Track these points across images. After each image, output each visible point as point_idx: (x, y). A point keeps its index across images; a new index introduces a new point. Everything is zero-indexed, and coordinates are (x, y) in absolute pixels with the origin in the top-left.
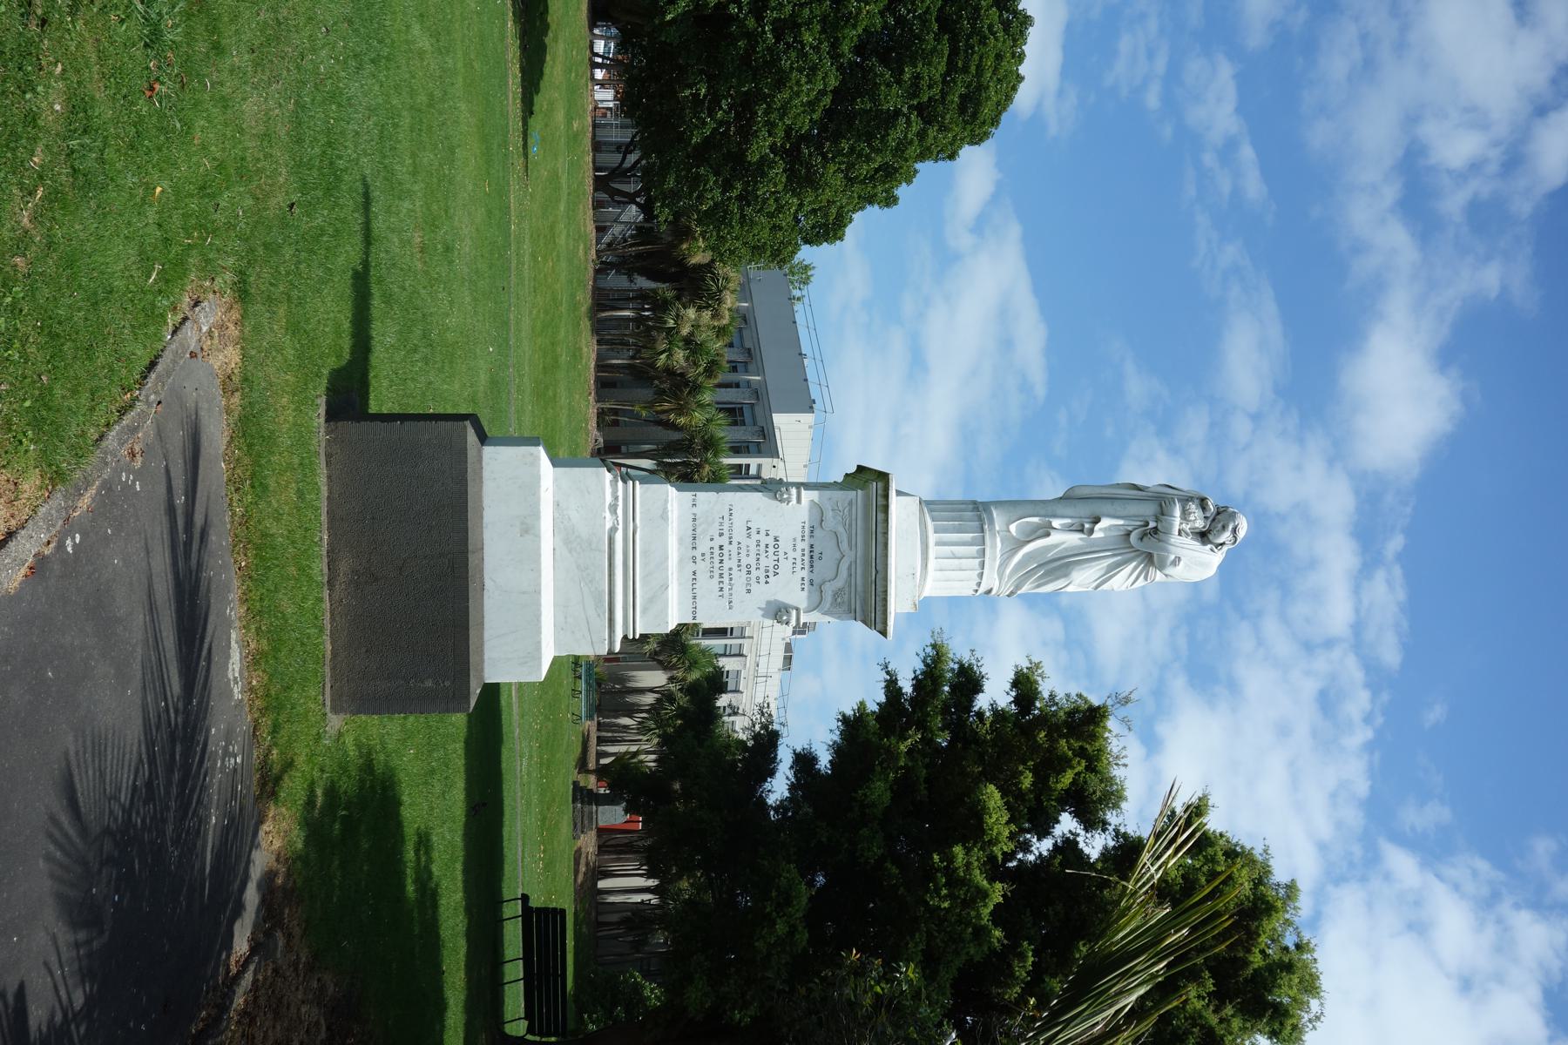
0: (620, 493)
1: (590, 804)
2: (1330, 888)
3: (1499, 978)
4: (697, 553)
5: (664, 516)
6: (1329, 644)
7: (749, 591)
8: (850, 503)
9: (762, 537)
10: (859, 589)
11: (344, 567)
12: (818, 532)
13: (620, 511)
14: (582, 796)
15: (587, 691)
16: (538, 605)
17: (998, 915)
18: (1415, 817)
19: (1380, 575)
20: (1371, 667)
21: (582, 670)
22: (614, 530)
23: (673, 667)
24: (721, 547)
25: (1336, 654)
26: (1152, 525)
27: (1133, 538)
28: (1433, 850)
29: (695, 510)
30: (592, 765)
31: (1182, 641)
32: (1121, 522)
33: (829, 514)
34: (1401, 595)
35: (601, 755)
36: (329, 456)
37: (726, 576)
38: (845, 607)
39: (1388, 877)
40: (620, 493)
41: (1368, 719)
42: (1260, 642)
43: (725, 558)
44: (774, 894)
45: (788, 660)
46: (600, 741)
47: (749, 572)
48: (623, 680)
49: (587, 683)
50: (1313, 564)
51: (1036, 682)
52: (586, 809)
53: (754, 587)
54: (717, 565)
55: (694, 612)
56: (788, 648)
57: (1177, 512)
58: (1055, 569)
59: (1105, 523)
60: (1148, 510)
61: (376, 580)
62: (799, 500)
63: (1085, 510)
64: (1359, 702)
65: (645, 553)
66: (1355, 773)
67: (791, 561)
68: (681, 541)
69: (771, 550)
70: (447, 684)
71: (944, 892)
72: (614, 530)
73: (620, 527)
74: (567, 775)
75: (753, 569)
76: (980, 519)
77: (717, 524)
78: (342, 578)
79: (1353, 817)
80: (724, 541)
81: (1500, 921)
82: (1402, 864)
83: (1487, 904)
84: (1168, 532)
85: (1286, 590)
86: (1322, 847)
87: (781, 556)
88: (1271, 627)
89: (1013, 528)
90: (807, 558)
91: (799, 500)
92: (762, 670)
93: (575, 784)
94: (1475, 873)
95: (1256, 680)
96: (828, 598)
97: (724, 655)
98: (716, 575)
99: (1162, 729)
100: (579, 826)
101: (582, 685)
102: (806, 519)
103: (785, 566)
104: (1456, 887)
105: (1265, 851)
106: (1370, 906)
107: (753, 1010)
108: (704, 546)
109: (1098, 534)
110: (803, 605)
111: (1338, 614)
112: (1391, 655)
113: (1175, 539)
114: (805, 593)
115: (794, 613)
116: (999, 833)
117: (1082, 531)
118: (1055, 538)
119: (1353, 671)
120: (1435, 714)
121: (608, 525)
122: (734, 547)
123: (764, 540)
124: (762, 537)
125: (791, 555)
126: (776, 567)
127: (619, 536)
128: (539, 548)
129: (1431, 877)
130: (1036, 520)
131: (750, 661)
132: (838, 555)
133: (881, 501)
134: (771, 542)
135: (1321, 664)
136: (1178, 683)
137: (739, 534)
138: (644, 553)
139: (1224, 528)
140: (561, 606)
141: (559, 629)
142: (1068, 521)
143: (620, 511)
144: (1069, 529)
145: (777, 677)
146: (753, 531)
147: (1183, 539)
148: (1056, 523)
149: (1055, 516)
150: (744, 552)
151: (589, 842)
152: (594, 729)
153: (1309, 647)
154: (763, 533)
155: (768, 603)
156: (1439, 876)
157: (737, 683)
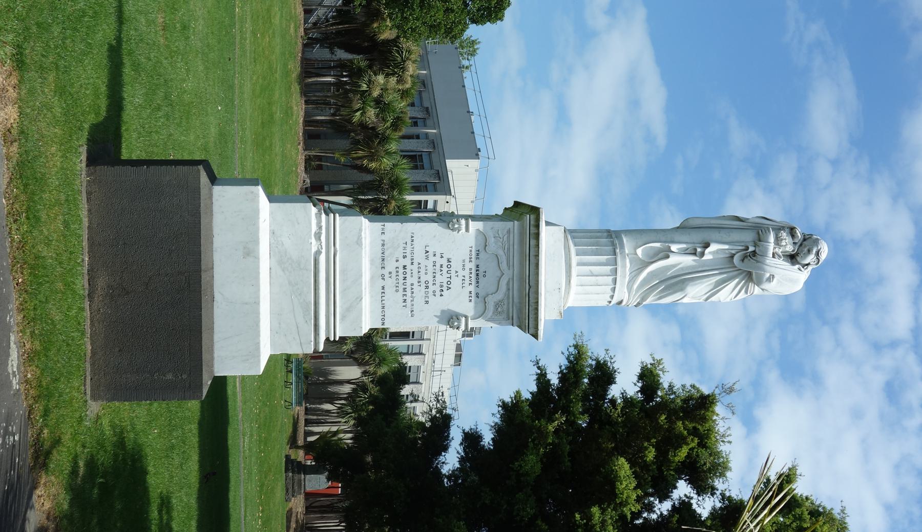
0: (323, 224)
1: (299, 473)
4: (386, 272)
5: (359, 242)
6: (894, 344)
7: (427, 302)
8: (509, 232)
10: (516, 300)
11: (101, 283)
12: (481, 255)
14: (292, 466)
15: (297, 382)
16: (257, 313)
22: (318, 253)
24: (404, 267)
25: (900, 352)
26: (751, 249)
27: (736, 260)
29: (383, 237)
30: (301, 442)
31: (775, 343)
32: (726, 247)
33: (491, 241)
36: (89, 194)
37: (409, 290)
38: (505, 316)
40: (323, 224)
43: (408, 276)
45: (458, 358)
47: (427, 287)
48: (326, 374)
49: (297, 376)
50: (881, 280)
51: (658, 375)
52: (296, 477)
54: (401, 281)
55: (383, 319)
56: (459, 347)
57: (772, 238)
59: (713, 247)
60: (748, 237)
61: (128, 293)
62: (467, 230)
63: (698, 237)
65: (343, 272)
68: (372, 262)
69: (445, 269)
72: (318, 253)
73: (324, 251)
74: (280, 450)
75: (430, 285)
76: (613, 244)
77: (401, 250)
78: (99, 292)
80: (407, 262)
84: (764, 255)
85: (859, 301)
87: (453, 274)
88: (847, 331)
89: (639, 251)
90: (473, 276)
91: (467, 230)
92: (437, 366)
93: (288, 457)
95: (835, 373)
97: (407, 354)
98: (401, 290)
100: (291, 490)
101: (293, 378)
102: (473, 244)
103: (456, 282)
105: (843, 511)
108: (391, 266)
109: (708, 256)
110: (470, 313)
113: (770, 260)
114: (472, 304)
115: (463, 319)
116: (628, 497)
117: (695, 254)
118: (673, 260)
123: (439, 261)
125: (461, 273)
126: (449, 283)
127: (322, 258)
131: (428, 358)
132: (499, 274)
133: (533, 230)
135: (887, 361)
136: (772, 376)
137: (419, 256)
139: (809, 251)
140: (276, 314)
141: (275, 332)
142: (684, 246)
144: (685, 252)
145: (449, 372)
146: (431, 254)
148: (674, 248)
149: (673, 242)
150: (423, 271)
152: (302, 413)
153: (877, 347)
154: (438, 255)
155: (443, 312)
157: (418, 376)
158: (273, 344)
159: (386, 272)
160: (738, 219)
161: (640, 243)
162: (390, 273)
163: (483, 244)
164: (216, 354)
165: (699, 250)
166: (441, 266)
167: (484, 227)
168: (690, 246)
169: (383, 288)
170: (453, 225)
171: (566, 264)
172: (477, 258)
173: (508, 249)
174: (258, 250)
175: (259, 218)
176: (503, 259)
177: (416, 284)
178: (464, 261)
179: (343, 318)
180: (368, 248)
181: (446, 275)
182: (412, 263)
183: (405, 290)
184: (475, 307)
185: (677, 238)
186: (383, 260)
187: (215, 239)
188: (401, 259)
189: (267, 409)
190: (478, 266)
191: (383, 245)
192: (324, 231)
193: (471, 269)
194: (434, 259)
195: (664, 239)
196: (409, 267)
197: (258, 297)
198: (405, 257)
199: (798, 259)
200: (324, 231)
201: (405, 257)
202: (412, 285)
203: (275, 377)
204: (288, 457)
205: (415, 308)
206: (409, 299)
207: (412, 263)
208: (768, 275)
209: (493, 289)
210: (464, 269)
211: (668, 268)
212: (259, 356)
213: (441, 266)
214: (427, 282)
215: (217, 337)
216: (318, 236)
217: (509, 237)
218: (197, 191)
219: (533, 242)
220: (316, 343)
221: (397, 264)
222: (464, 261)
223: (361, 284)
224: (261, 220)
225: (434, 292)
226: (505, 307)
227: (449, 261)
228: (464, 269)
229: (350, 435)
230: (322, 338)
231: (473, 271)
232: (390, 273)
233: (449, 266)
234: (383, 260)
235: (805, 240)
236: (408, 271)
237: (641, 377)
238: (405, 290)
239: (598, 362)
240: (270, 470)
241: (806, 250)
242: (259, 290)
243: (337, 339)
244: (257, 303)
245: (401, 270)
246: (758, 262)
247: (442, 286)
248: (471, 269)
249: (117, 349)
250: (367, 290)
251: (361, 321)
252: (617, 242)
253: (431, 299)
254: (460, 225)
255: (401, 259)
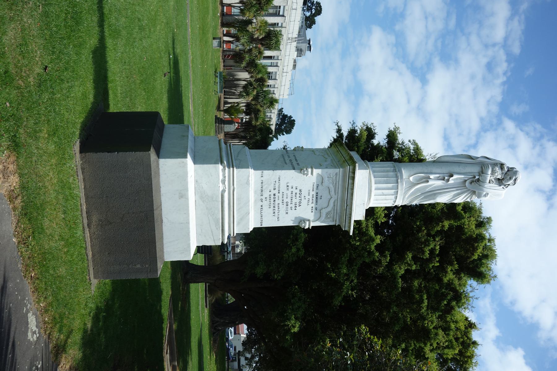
0: (227, 175)
1: (221, 124)
2: (482, 133)
3: (538, 165)
4: (263, 198)
5: (248, 183)
6: (494, 45)
7: (287, 213)
8: (336, 174)
9: (294, 190)
10: (338, 211)
11: (95, 219)
12: (320, 187)
13: (227, 183)
14: (219, 121)
15: (220, 82)
16: (188, 228)
17: (378, 247)
18: (516, 109)
19: (516, 19)
20: (509, 55)
21: (218, 75)
22: (224, 191)
23: (252, 73)
24: (274, 195)
25: (497, 48)
26: (477, 177)
27: (467, 183)
28: (521, 121)
29: (262, 179)
30: (222, 108)
31: (439, 44)
32: (463, 176)
33: (326, 179)
34: (523, 27)
35: (226, 103)
36: (83, 169)
37: (276, 207)
38: (331, 219)
39: (504, 129)
40: (227, 175)
41: (505, 74)
42: (469, 44)
43: (276, 199)
44: (291, 237)
45: (295, 66)
46: (225, 98)
47: (287, 205)
48: (233, 75)
49: (220, 79)
50: (493, 14)
51: (396, 135)
52: (220, 126)
53: (290, 211)
54: (272, 202)
55: (261, 223)
56: (295, 61)
57: (490, 172)
58: (430, 195)
59: (455, 177)
60: (475, 170)
61: (111, 223)
62: (312, 173)
63: (446, 170)
64: (502, 67)
65: (238, 199)
66: (496, 92)
67: (307, 200)
68: (255, 192)
69: (298, 195)
70: (147, 266)
71: (358, 238)
72: (224, 191)
73: (227, 190)
74: (213, 113)
75: (289, 204)
76: (397, 177)
77: (272, 185)
78: (94, 223)
79: (495, 109)
80: (276, 192)
81: (541, 145)
82: (510, 125)
83: (537, 140)
84: (484, 182)
85: (481, 24)
86: (482, 119)
87: (303, 198)
88: (474, 38)
89: (411, 178)
90: (314, 199)
91: (312, 173)
92: (285, 70)
93: (216, 116)
94: (535, 129)
95: (465, 59)
96: (324, 215)
97: (271, 66)
98: (272, 207)
99: (428, 76)
100: (217, 132)
101: (218, 80)
102: (315, 181)
103: (304, 202)
104: (527, 134)
105: (481, 204)
106: (496, 139)
107: (282, 274)
108: (266, 194)
109: (452, 181)
110: (312, 218)
111: (499, 34)
112: (516, 49)
113: (487, 185)
114: (313, 213)
115: (308, 223)
116: (380, 215)
117: (444, 179)
118: (431, 182)
119: (502, 55)
120: (530, 72)
121: (221, 189)
122: (281, 195)
123: (295, 191)
124: (294, 190)
125: (307, 197)
126: (300, 202)
127: (226, 195)
128: (188, 204)
129: (520, 132)
130: (423, 175)
131: (281, 68)
132: (329, 197)
133: (351, 175)
134: (298, 192)
135: (490, 52)
136: (436, 60)
137: (283, 189)
138: (238, 199)
139: (510, 179)
140: (199, 225)
141: (198, 234)
142: (438, 175)
143: (227, 183)
144: (438, 179)
145: (290, 73)
146: (290, 187)
147: (491, 185)
148: (432, 177)
149: (432, 173)
150: (285, 196)
151: (222, 136)
152: (222, 94)
153: (486, 46)
154: (294, 188)
155: (296, 218)
156: (522, 130)
157: (276, 76)
158: (198, 240)
159: (263, 198)
160: (470, 157)
161: (412, 174)
162: (266, 198)
163: (321, 181)
164: (165, 250)
165: (446, 178)
166: (296, 194)
167: (322, 172)
168: (441, 175)
169: (262, 206)
170: (304, 172)
171: (369, 189)
172: (317, 189)
173: (336, 184)
174: (188, 194)
175: (187, 177)
176: (332, 189)
177: (281, 204)
178: (309, 191)
179: (238, 224)
180: (253, 186)
181: (298, 198)
182: (279, 193)
183: (274, 207)
184: (315, 215)
185: (434, 170)
186: (262, 191)
187: (161, 189)
188: (272, 190)
189: (206, 98)
190: (317, 193)
191: (262, 183)
192: (227, 179)
193: (313, 195)
194: (292, 190)
195: (426, 171)
196: (277, 195)
197: (189, 220)
198: (275, 189)
199: (503, 182)
200: (227, 179)
201: (275, 189)
202: (279, 204)
203: (210, 82)
204: (216, 116)
205: (280, 216)
206: (276, 211)
207: (279, 193)
208: (485, 193)
209: (326, 205)
210: (309, 195)
211: (427, 187)
212: (190, 251)
213: (296, 194)
214: (287, 203)
215: (165, 241)
216: (223, 182)
217: (336, 177)
218: (149, 166)
219: (350, 181)
220: (223, 239)
221: (270, 193)
222: (309, 191)
223: (249, 206)
224: (189, 175)
225: (291, 207)
226: (332, 215)
227: (300, 191)
228: (309, 195)
229: (244, 104)
230: (226, 235)
231: (315, 196)
232: (266, 198)
233: (300, 194)
234: (262, 191)
235: (508, 171)
236: (276, 197)
237: (388, 136)
238: (274, 207)
239: (367, 127)
240: (208, 125)
241: (508, 177)
242: (189, 216)
243: (235, 235)
244: (188, 223)
245: (272, 196)
246: (480, 185)
247: (296, 204)
248: (313, 195)
249: (107, 253)
250: (253, 208)
251: (249, 225)
252: (399, 175)
253: (289, 211)
254: (308, 172)
255: (272, 190)
